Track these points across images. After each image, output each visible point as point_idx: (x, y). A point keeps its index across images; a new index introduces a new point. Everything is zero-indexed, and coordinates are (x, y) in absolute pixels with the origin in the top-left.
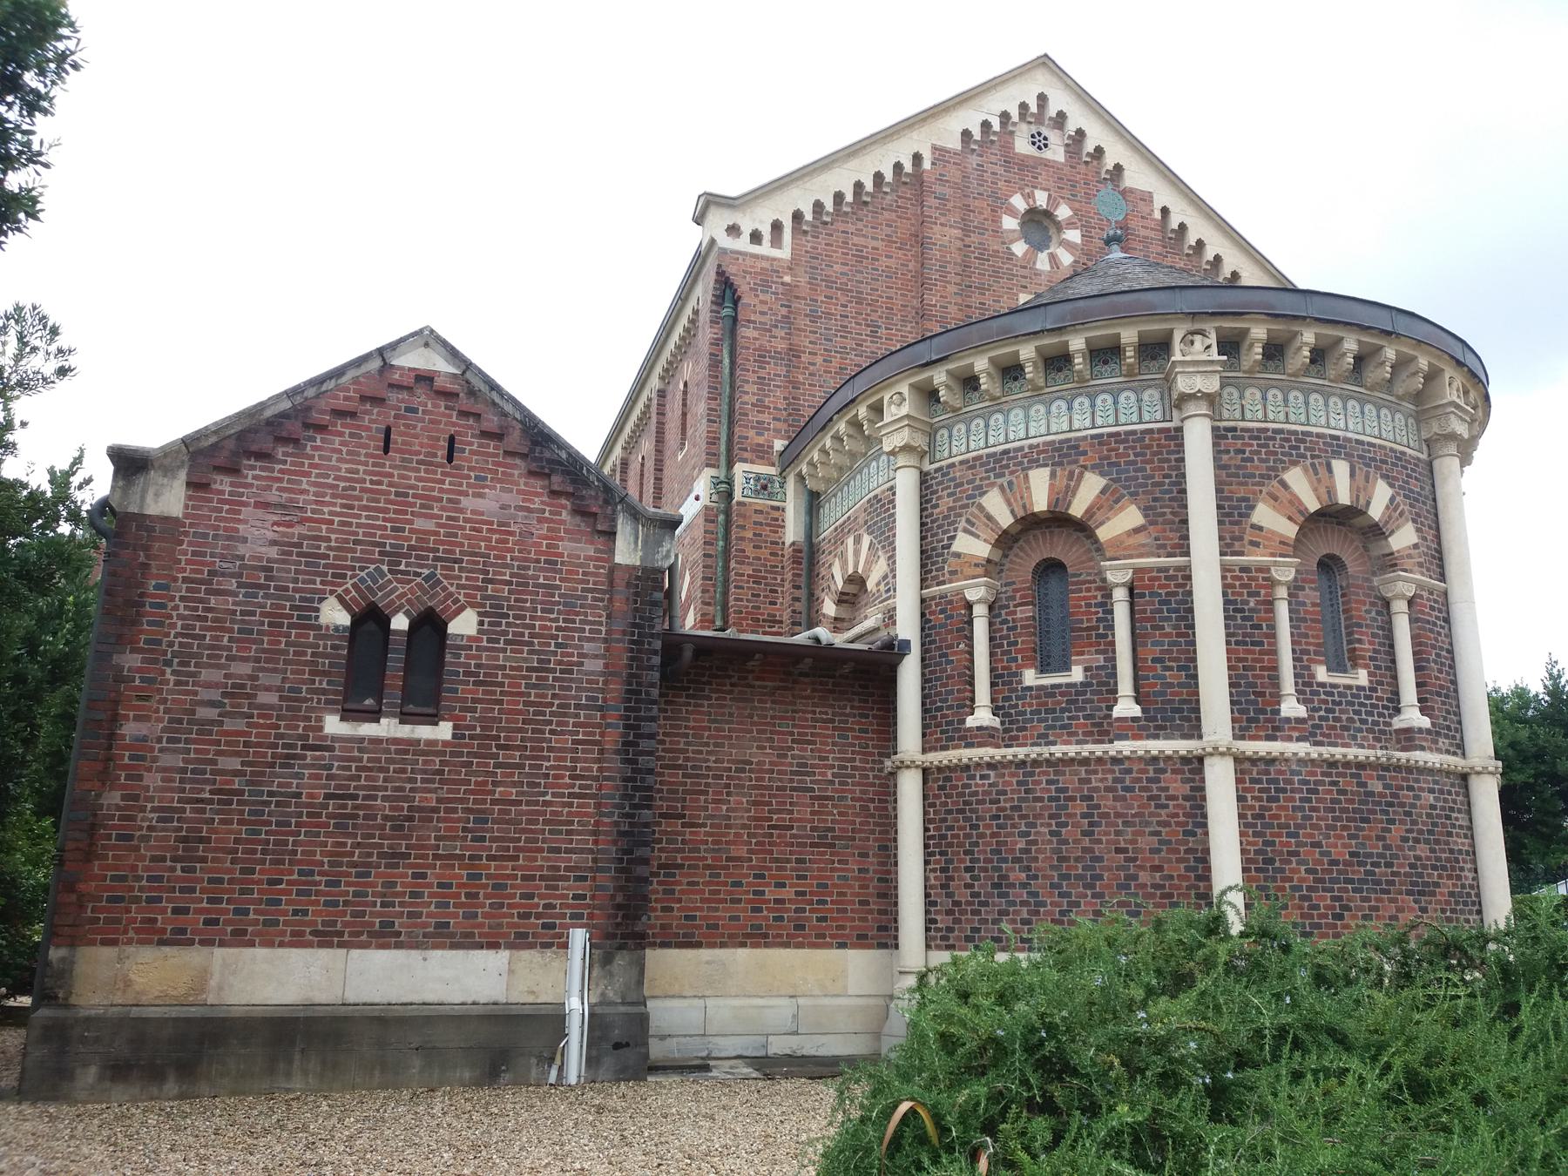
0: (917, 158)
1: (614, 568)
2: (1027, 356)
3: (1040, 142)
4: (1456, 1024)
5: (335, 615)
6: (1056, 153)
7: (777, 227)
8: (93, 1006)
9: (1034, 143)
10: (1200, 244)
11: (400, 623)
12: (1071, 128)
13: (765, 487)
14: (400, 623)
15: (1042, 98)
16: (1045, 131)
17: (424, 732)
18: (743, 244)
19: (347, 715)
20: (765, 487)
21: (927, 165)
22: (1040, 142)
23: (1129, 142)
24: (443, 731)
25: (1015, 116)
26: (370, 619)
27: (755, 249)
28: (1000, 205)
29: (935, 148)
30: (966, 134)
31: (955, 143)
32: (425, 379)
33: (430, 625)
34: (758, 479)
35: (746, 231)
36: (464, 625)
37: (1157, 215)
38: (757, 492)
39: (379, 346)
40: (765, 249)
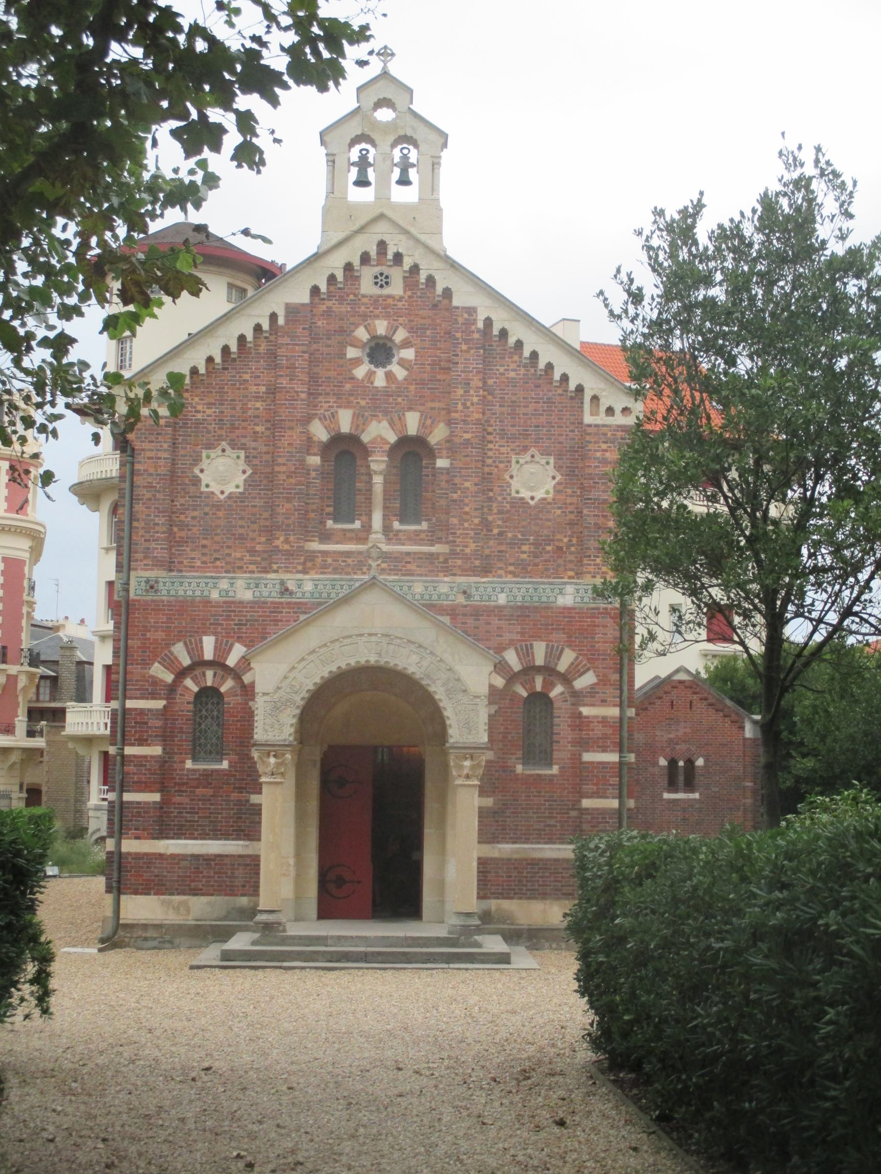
0: (273, 317)
1: (745, 739)
2: (313, 458)
3: (382, 281)
5: (663, 762)
6: (396, 288)
8: (441, 866)
9: (376, 283)
10: (550, 367)
13: (152, 587)
15: (382, 245)
17: (691, 796)
19: (195, 759)
21: (281, 321)
22: (382, 281)
23: (559, 344)
24: (696, 796)
25: (356, 262)
26: (673, 763)
29: (287, 306)
30: (315, 290)
31: (305, 298)
32: (681, 682)
33: (690, 762)
34: (147, 582)
36: (700, 762)
37: (480, 325)
39: (114, 569)
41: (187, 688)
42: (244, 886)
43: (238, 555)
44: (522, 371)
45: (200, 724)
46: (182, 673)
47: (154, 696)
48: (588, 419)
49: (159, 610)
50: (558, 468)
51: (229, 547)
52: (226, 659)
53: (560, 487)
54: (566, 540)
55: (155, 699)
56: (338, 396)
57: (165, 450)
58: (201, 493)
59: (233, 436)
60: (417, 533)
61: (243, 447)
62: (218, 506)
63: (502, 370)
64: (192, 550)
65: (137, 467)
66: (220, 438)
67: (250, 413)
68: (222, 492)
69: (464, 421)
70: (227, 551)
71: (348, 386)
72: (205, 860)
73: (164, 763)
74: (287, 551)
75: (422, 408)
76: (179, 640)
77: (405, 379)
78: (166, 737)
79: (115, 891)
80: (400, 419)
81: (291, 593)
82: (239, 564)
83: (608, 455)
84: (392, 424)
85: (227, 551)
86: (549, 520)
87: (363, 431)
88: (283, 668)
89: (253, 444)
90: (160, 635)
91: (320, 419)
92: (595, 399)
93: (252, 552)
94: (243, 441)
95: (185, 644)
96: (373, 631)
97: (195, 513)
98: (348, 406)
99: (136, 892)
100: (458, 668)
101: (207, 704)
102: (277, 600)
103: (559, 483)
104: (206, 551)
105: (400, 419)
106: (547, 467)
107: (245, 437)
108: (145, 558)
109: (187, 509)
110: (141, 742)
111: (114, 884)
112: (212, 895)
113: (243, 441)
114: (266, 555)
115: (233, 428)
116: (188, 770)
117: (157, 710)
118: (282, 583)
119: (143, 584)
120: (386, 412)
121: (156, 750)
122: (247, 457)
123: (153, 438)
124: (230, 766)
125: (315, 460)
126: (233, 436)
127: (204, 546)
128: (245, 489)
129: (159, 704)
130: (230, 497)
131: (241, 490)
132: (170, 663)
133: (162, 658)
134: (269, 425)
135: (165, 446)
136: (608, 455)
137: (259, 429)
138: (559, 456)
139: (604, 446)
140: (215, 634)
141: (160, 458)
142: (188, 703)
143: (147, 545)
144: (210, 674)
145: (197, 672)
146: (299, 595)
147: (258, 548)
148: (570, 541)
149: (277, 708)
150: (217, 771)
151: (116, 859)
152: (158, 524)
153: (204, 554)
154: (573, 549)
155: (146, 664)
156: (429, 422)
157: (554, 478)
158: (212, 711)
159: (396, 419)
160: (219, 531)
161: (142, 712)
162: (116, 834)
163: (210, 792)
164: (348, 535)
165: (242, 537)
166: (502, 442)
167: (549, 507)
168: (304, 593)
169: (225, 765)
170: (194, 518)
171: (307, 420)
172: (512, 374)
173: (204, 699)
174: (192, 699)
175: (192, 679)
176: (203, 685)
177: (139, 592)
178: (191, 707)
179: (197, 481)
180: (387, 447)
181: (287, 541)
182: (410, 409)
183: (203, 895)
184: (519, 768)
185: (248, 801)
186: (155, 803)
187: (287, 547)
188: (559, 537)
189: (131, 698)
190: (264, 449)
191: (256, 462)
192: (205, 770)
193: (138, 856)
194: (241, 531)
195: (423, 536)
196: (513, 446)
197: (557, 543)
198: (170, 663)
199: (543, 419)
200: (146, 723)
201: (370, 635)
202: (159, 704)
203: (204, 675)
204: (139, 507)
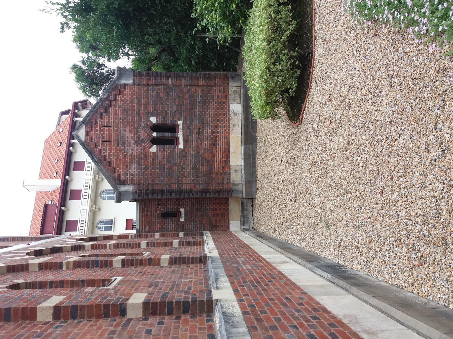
5: (154, 149)
11: (155, 134)
26: (154, 141)
33: (155, 128)
36: (153, 120)
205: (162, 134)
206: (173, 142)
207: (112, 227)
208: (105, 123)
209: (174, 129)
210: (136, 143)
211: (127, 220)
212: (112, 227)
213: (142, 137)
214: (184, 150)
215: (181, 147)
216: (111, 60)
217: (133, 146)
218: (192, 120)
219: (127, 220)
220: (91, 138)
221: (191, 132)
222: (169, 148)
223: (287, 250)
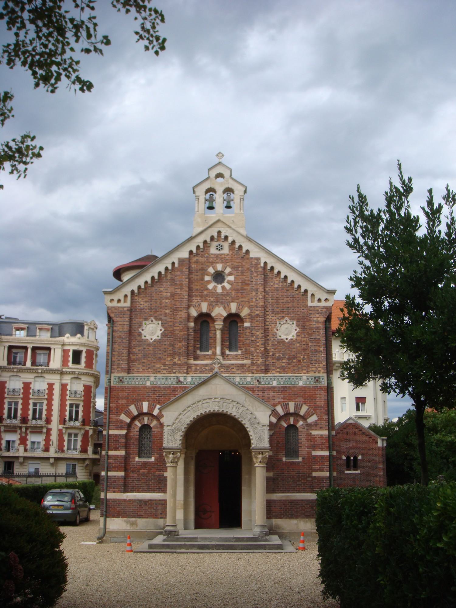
0: (173, 264)
4: (128, 601)
5: (344, 458)
6: (226, 250)
7: (126, 296)
11: (352, 458)
12: (230, 240)
14: (352, 458)
15: (219, 232)
16: (222, 243)
18: (115, 304)
20: (317, 381)
26: (348, 458)
27: (119, 305)
28: (204, 271)
33: (355, 458)
35: (116, 299)
36: (360, 457)
37: (262, 265)
38: (315, 382)
40: (122, 304)
41: (136, 425)
42: (161, 514)
43: (158, 366)
44: (281, 284)
45: (142, 441)
46: (134, 419)
47: (121, 428)
48: (310, 304)
49: (124, 390)
50: (297, 325)
51: (154, 363)
52: (153, 412)
53: (299, 334)
54: (302, 357)
55: (122, 430)
56: (201, 296)
57: (127, 321)
58: (142, 339)
59: (156, 315)
60: (236, 355)
61: (160, 319)
62: (149, 345)
63: (272, 284)
64: (138, 364)
65: (115, 328)
66: (151, 316)
67: (163, 305)
68: (151, 339)
69: (256, 306)
70: (153, 364)
71: (205, 293)
72: (144, 502)
73: (126, 458)
74: (179, 364)
75: (237, 301)
76: (132, 404)
77: (230, 289)
78: (127, 447)
79: (104, 516)
80: (228, 306)
81: (181, 382)
82: (159, 370)
83: (319, 319)
84: (225, 308)
85: (153, 364)
86: (294, 348)
87: (212, 311)
88: (177, 414)
89: (165, 318)
90: (124, 402)
91: (193, 307)
92: (313, 295)
93: (164, 365)
94: (161, 317)
95: (135, 405)
96: (217, 397)
97: (140, 348)
98: (206, 300)
99: (114, 517)
100: (255, 412)
101: (145, 432)
102: (175, 385)
103: (298, 332)
104: (144, 364)
105: (228, 306)
106: (293, 325)
107: (161, 315)
108: (118, 368)
109: (136, 347)
110: (116, 449)
111: (104, 513)
112: (147, 518)
113: (161, 317)
114: (170, 366)
115: (156, 311)
116: (137, 461)
117: (123, 435)
118: (178, 378)
119: (117, 379)
120: (222, 303)
121: (122, 453)
122: (162, 324)
123: (121, 316)
124: (155, 460)
125: (192, 324)
126: (156, 315)
127: (144, 363)
128: (161, 338)
129: (124, 432)
130: (155, 341)
131: (159, 338)
132: (128, 414)
133: (125, 412)
134: (171, 310)
135: (127, 319)
136: (319, 319)
137: (167, 311)
138: (298, 321)
139: (318, 315)
140: (148, 401)
141: (125, 325)
142: (137, 432)
143: (119, 362)
144: (146, 419)
145: (141, 418)
146: (185, 383)
147: (167, 363)
148: (304, 357)
149: (174, 432)
150: (149, 462)
151: (105, 501)
152: (123, 353)
153: (143, 366)
154: (305, 361)
155: (118, 414)
156: (241, 307)
157: (296, 330)
158: (147, 435)
159: (226, 306)
160: (150, 356)
161: (116, 436)
162: (105, 491)
163: (146, 471)
164: (207, 357)
165: (160, 358)
166: (273, 315)
167: (294, 342)
168: (187, 382)
169: (153, 459)
170: (139, 350)
171: (189, 307)
172: (276, 286)
173: (144, 430)
174: (138, 430)
175: (138, 421)
176: (143, 424)
177: (115, 383)
178: (138, 433)
179: (140, 334)
180: (223, 318)
181: (179, 360)
182: (232, 302)
183: (143, 518)
184: (284, 459)
185: (163, 475)
186: (122, 476)
187: (179, 362)
188: (298, 355)
189: (111, 429)
190: (169, 320)
191: (166, 325)
192: (144, 461)
193: (114, 500)
194: (160, 356)
195: (239, 357)
196: (277, 316)
197: (298, 358)
198: (128, 414)
199: (290, 305)
200: (118, 441)
201: (215, 398)
202: (124, 432)
203: (143, 419)
204: (116, 346)
205: (352, 462)
206: (348, 468)
207: (163, 503)
208: (357, 432)
209: (355, 468)
210: (347, 448)
211: (365, 398)
212: (163, 503)
213: (350, 451)
214: (344, 474)
215: (346, 472)
216: (18, 62)
217: (345, 446)
218: (360, 478)
219: (365, 398)
220: (349, 426)
221: (354, 478)
222: (345, 466)
223: (276, 546)
